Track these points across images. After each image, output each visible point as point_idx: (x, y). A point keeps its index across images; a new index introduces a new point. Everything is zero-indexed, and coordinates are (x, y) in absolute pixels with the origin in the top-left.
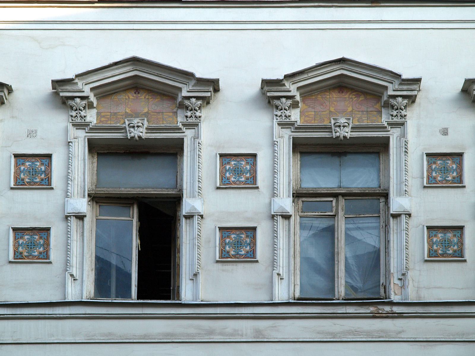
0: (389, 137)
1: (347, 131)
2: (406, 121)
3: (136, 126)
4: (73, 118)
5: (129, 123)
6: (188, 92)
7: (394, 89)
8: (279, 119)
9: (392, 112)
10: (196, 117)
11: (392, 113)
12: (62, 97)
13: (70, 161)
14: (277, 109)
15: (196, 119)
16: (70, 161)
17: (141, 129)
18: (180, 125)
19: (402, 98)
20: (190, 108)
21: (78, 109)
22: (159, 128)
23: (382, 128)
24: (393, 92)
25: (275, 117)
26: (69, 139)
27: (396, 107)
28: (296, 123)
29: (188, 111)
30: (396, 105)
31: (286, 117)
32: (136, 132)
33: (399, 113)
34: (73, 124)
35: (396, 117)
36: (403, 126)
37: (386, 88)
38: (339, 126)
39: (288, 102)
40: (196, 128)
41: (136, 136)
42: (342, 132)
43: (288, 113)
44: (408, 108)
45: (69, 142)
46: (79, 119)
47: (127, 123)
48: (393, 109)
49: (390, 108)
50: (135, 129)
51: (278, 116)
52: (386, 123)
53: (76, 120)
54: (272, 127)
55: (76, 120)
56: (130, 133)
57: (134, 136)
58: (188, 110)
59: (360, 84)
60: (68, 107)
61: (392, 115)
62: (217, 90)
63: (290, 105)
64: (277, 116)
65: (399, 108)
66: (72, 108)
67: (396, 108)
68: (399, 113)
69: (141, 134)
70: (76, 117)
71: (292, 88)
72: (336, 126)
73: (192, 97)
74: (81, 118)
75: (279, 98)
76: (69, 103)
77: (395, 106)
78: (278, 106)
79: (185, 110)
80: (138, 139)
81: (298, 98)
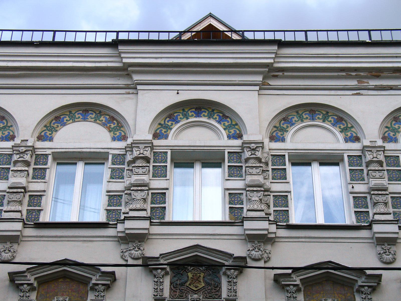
4: (21, 297)
6: (362, 282)
7: (362, 281)
8: (21, 298)
10: (293, 297)
11: (288, 295)
12: (16, 284)
14: (288, 292)
15: (293, 299)
19: (293, 286)
20: (364, 292)
21: (292, 292)
24: (361, 283)
27: (364, 292)
30: (23, 289)
31: (294, 298)
33: (25, 294)
37: (91, 279)
39: (295, 288)
43: (28, 294)
44: (372, 293)
46: (292, 299)
49: (286, 292)
51: (364, 298)
53: (291, 299)
55: (291, 299)
58: (21, 292)
59: (79, 277)
60: (285, 290)
62: (115, 280)
63: (370, 291)
65: (366, 293)
66: (21, 290)
68: (25, 294)
70: (23, 297)
71: (31, 279)
73: (365, 286)
74: (293, 298)
75: (289, 285)
76: (286, 288)
79: (360, 293)
81: (35, 285)
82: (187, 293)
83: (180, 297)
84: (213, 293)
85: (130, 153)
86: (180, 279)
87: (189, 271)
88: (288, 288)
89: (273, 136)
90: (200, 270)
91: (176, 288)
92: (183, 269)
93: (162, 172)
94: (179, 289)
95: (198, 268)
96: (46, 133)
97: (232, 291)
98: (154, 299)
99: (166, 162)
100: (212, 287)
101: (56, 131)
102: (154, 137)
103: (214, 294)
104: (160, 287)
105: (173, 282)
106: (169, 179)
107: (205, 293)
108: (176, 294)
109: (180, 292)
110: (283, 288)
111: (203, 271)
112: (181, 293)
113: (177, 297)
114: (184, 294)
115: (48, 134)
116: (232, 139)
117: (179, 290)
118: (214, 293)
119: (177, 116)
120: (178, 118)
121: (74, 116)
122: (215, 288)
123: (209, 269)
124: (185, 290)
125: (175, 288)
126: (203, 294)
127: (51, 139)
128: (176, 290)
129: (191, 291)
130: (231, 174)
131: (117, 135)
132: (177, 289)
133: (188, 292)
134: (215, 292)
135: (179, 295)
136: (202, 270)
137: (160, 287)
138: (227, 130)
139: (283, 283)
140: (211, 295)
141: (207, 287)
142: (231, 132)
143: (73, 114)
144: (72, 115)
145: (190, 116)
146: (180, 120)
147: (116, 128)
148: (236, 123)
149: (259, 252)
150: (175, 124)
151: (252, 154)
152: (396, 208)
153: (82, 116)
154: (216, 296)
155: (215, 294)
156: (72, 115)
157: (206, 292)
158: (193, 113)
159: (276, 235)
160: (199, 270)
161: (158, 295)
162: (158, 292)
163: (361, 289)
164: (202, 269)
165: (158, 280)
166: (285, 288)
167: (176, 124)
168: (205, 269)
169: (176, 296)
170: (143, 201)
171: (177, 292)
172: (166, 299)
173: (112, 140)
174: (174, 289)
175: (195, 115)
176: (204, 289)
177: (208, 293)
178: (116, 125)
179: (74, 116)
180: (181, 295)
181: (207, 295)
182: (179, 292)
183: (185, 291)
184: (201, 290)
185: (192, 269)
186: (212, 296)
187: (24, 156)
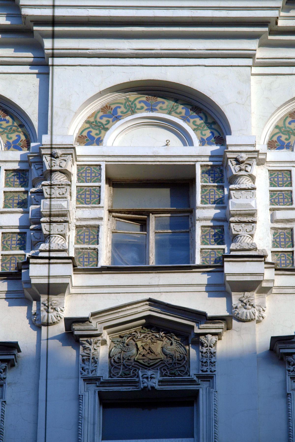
0: (198, 390)
1: (155, 382)
2: (215, 375)
3: (149, 377)
5: (142, 374)
9: (289, 367)
11: (289, 369)
13: (81, 406)
14: (290, 365)
16: (81, 406)
17: (154, 380)
18: (194, 377)
20: (292, 363)
22: (184, 380)
23: (192, 382)
25: (287, 372)
26: (288, 391)
27: (292, 363)
28: (215, 375)
29: (290, 367)
30: (293, 361)
32: (149, 383)
34: (198, 376)
35: (293, 372)
36: (212, 379)
38: (147, 378)
40: (211, 380)
41: (149, 387)
42: (149, 383)
45: (288, 394)
47: (141, 374)
48: (290, 365)
50: (148, 380)
52: (195, 376)
54: (285, 381)
56: (143, 383)
57: (147, 386)
61: (289, 371)
64: (289, 371)
67: (292, 364)
69: (154, 385)
72: (143, 378)
76: (287, 359)
77: (291, 362)
78: (290, 362)
80: (150, 389)
82: (136, 370)
83: (124, 376)
84: (176, 368)
85: (37, 167)
86: (124, 351)
87: (138, 340)
88: (290, 359)
89: (273, 141)
90: (156, 337)
91: (119, 363)
92: (130, 337)
93: (93, 196)
94: (124, 365)
95: (153, 335)
96: (91, 132)
97: (209, 364)
98: (289, 378)
99: (100, 181)
100: (175, 361)
101: (107, 129)
102: (222, 137)
103: (177, 371)
104: (210, 360)
105: (113, 356)
106: (103, 207)
107: (164, 369)
108: (119, 372)
109: (124, 369)
110: (282, 359)
111: (160, 338)
112: (126, 371)
113: (121, 375)
114: (130, 371)
115: (93, 134)
116: (12, 148)
117: (124, 367)
118: (177, 369)
119: (116, 108)
120: (117, 113)
121: (133, 105)
122: (179, 362)
123: (168, 336)
124: (133, 366)
125: (117, 363)
126: (161, 371)
127: (99, 142)
128: (118, 366)
129: (142, 367)
130: (80, 199)
131: (96, 139)
132: (120, 365)
133: (136, 369)
134: (179, 368)
135: (124, 373)
136: (158, 338)
137: (210, 360)
138: (199, 132)
139: (282, 351)
140: (173, 372)
141: (167, 361)
142: (11, 138)
143: (130, 101)
144: (130, 103)
145: (138, 109)
146: (121, 114)
147: (11, 128)
148: (214, 121)
149: (53, 312)
150: (113, 121)
151: (240, 170)
152: (278, 246)
153: (147, 106)
154: (181, 372)
155: (179, 371)
156: (130, 103)
157: (165, 368)
158: (142, 104)
159: (274, 284)
160: (154, 337)
161: (209, 371)
162: (207, 366)
163: (287, 359)
164: (159, 335)
165: (207, 350)
166: (284, 359)
167: (115, 122)
168: (164, 335)
169: (118, 374)
170: (62, 240)
171: (120, 369)
172: (102, 378)
173: (6, 146)
174: (116, 365)
175: (146, 107)
176: (162, 363)
177: (168, 369)
178: (10, 124)
179: (133, 105)
180: (127, 372)
181: (167, 372)
182: (123, 369)
183: (133, 368)
184: (158, 366)
185: (144, 337)
186: (175, 372)
187: (246, 168)
